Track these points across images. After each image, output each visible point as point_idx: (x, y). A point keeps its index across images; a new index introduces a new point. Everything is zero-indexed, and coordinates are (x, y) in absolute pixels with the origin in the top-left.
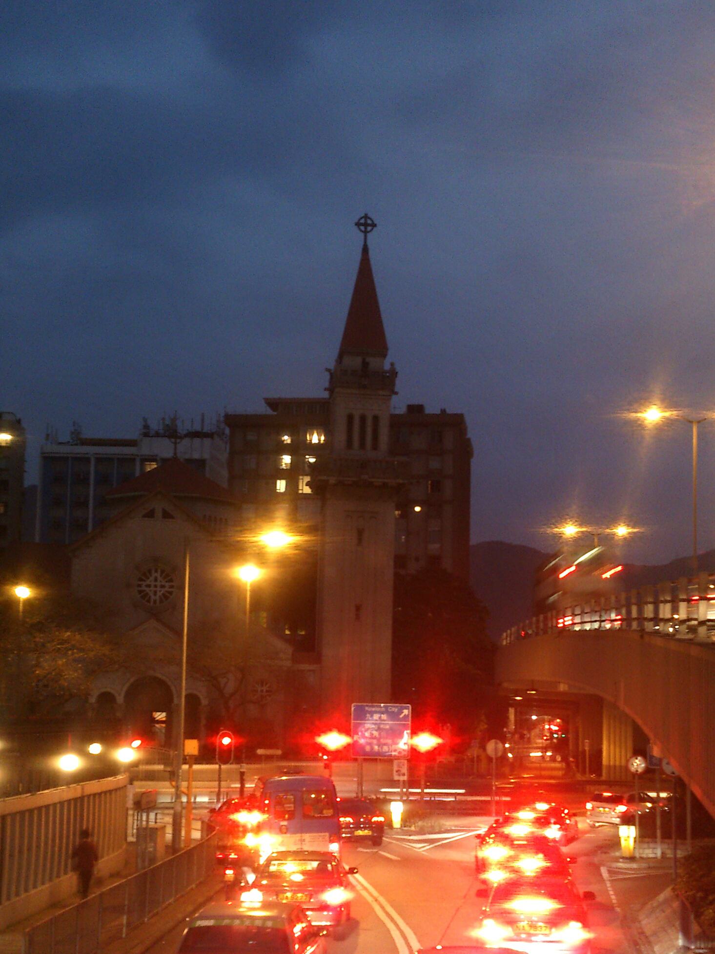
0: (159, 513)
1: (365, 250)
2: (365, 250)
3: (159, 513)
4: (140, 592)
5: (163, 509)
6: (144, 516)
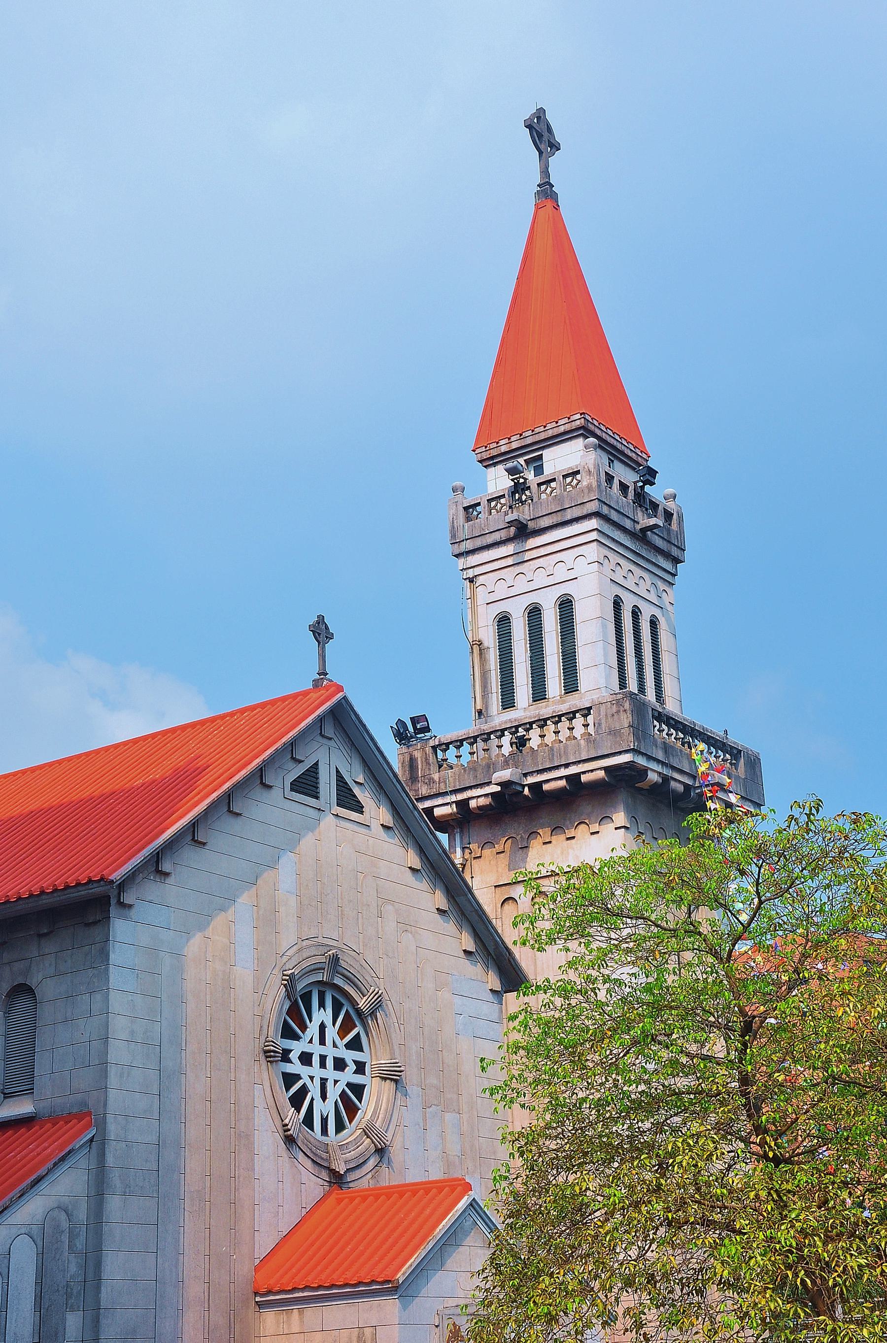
5: (317, 764)
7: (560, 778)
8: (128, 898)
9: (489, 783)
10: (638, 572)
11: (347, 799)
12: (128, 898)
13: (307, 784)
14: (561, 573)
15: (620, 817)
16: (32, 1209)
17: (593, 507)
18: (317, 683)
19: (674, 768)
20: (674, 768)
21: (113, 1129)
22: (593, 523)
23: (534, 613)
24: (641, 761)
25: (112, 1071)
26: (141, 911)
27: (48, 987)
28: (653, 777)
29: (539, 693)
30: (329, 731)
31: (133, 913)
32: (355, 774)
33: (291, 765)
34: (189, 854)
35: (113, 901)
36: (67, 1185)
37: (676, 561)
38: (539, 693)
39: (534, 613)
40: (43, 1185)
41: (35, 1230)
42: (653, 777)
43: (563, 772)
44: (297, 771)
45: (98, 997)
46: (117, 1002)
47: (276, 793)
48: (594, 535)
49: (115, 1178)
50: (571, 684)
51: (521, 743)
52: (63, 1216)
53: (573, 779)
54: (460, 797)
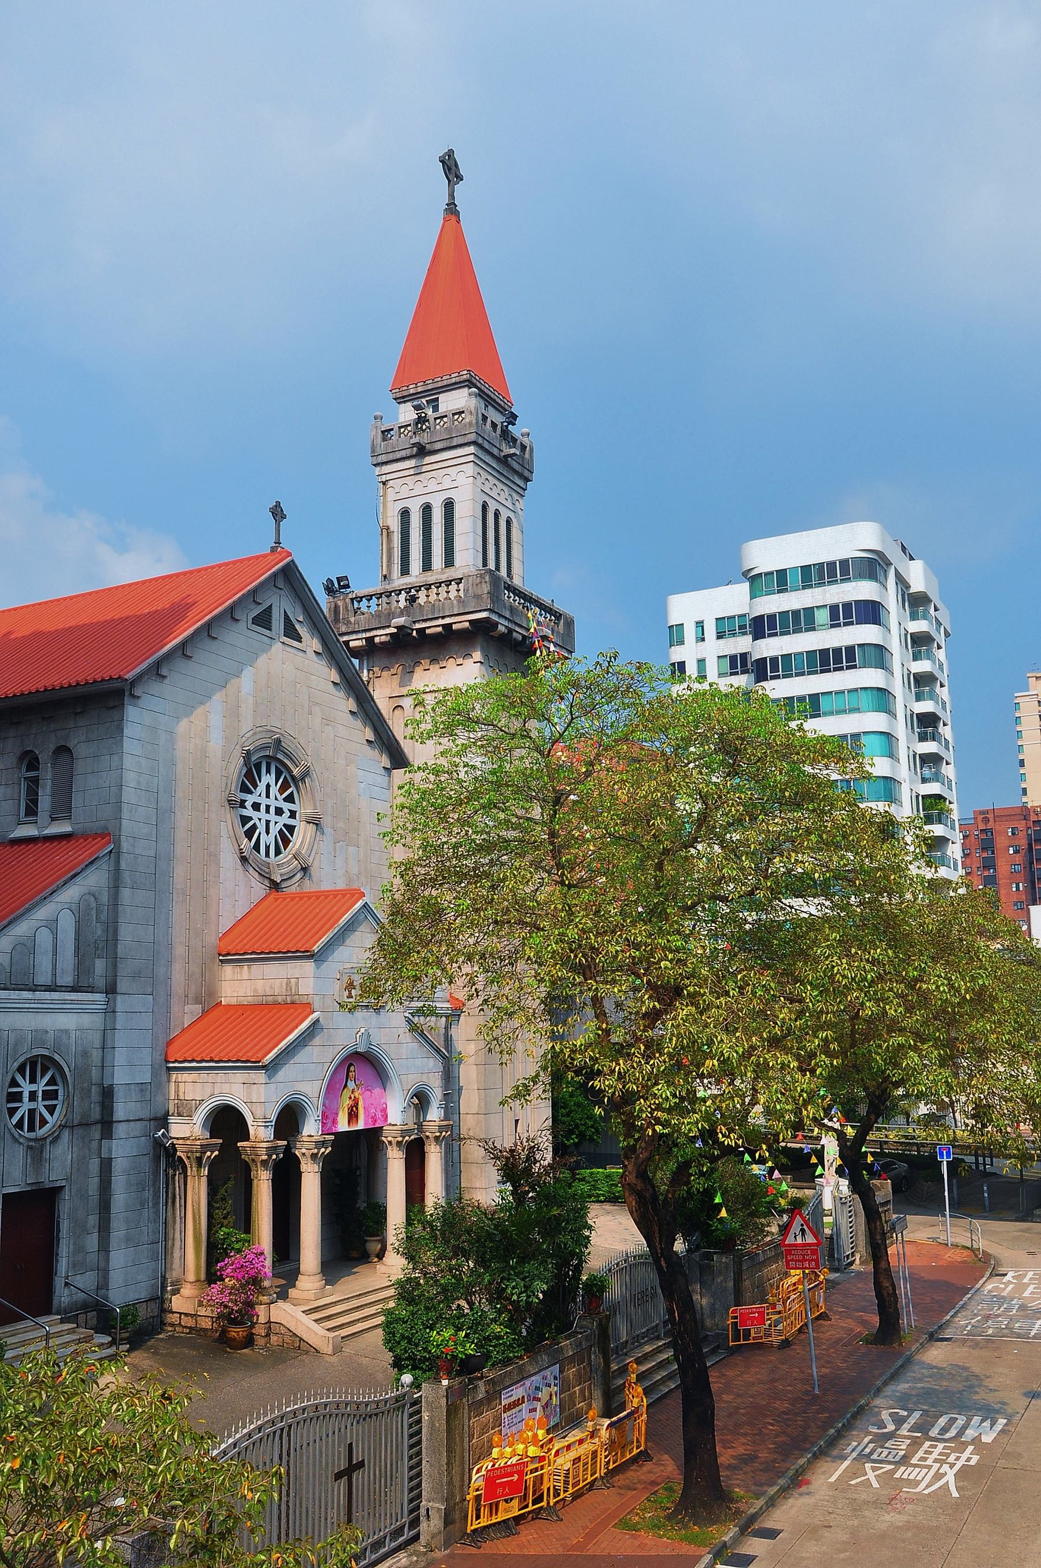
1: (452, 209)
2: (452, 209)
7: (438, 626)
9: (389, 626)
10: (500, 486)
11: (291, 632)
12: (137, 692)
13: (263, 620)
14: (447, 483)
15: (477, 655)
16: (71, 893)
17: (472, 437)
18: (273, 550)
19: (516, 624)
20: (516, 624)
21: (125, 846)
22: (472, 449)
23: (427, 509)
24: (494, 617)
25: (125, 808)
26: (146, 701)
27: (81, 750)
28: (501, 629)
29: (427, 566)
30: (281, 583)
31: (140, 702)
32: (297, 616)
33: (253, 606)
34: (180, 664)
35: (127, 693)
36: (95, 879)
37: (527, 480)
38: (427, 566)
39: (427, 509)
40: (78, 879)
41: (74, 906)
42: (501, 629)
43: (441, 622)
44: (257, 611)
45: (115, 757)
46: (128, 762)
47: (242, 625)
48: (472, 458)
49: (126, 877)
50: (449, 562)
51: (413, 600)
52: (92, 899)
53: (447, 627)
54: (368, 635)
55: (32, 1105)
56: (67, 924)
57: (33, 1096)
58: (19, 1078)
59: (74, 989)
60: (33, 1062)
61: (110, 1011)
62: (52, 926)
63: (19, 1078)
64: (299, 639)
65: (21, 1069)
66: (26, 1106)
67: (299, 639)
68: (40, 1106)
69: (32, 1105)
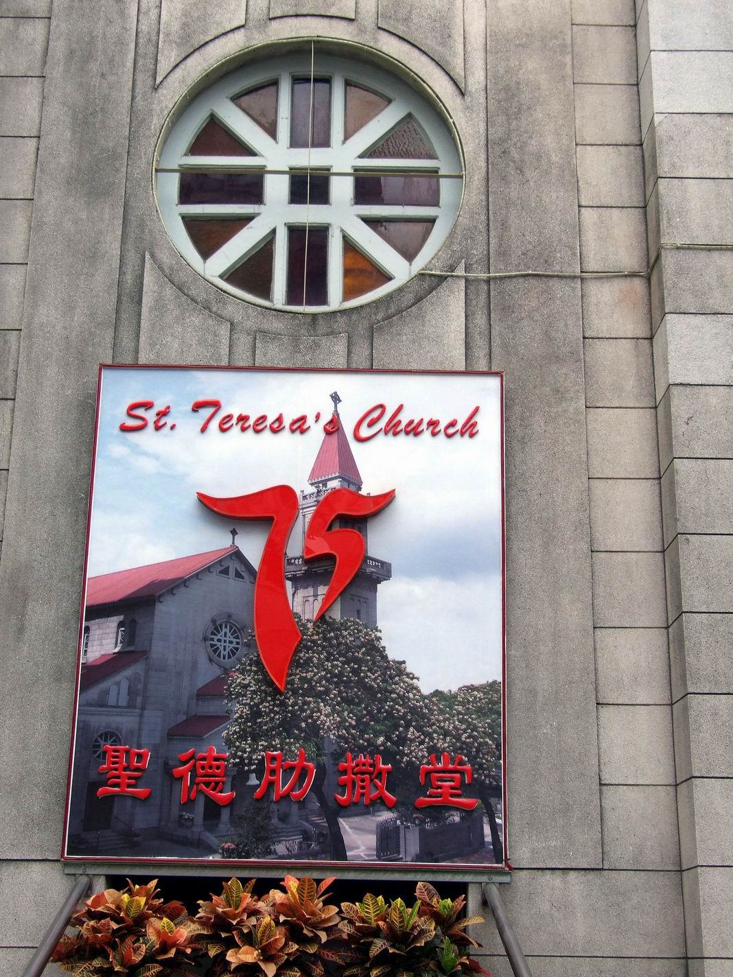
0: (232, 572)
3: (232, 572)
4: (229, 657)
6: (220, 572)
8: (161, 600)
11: (238, 575)
13: (225, 572)
18: (231, 545)
32: (241, 569)
34: (182, 589)
55: (342, 189)
56: (125, 685)
57: (311, 187)
58: (99, 739)
59: (126, 708)
60: (106, 734)
61: (141, 716)
62: (118, 684)
63: (99, 739)
64: (243, 578)
65: (101, 736)
66: (276, 213)
67: (243, 578)
68: (341, 215)
69: (342, 189)
